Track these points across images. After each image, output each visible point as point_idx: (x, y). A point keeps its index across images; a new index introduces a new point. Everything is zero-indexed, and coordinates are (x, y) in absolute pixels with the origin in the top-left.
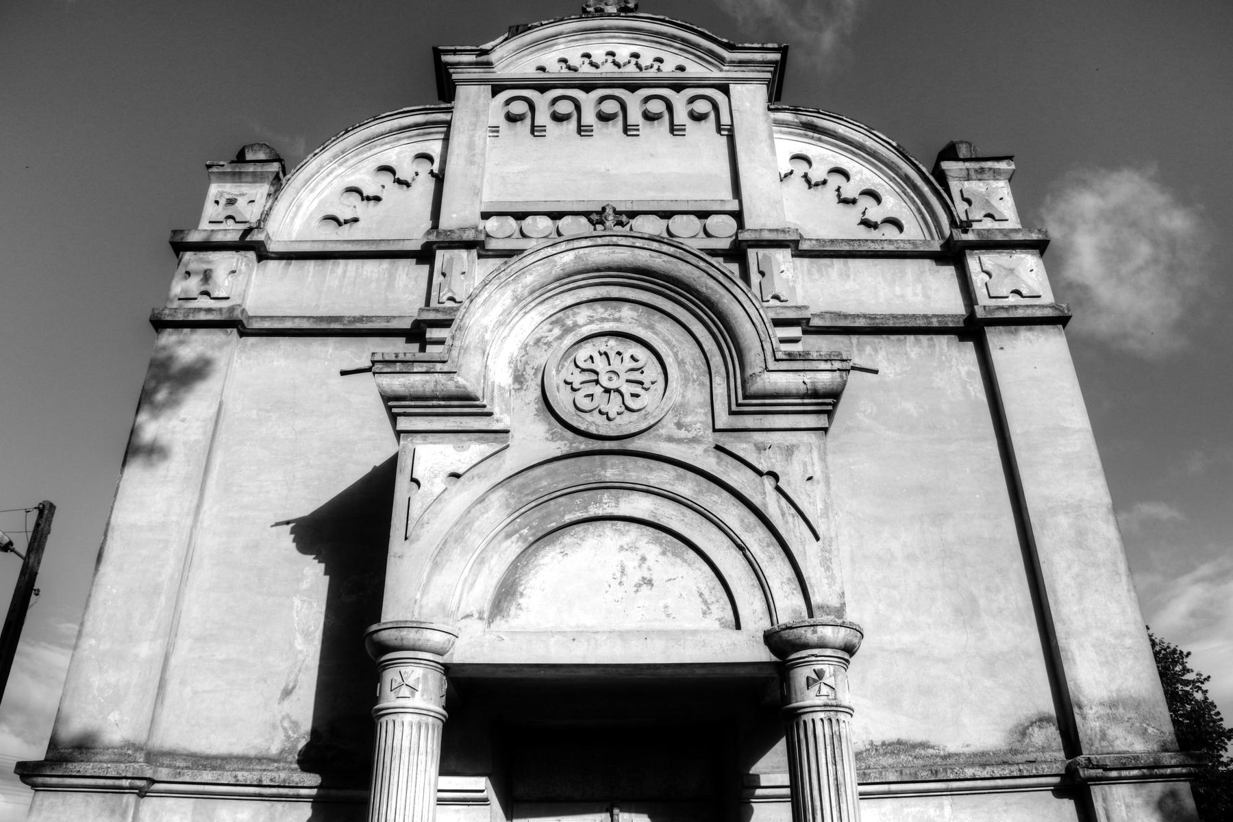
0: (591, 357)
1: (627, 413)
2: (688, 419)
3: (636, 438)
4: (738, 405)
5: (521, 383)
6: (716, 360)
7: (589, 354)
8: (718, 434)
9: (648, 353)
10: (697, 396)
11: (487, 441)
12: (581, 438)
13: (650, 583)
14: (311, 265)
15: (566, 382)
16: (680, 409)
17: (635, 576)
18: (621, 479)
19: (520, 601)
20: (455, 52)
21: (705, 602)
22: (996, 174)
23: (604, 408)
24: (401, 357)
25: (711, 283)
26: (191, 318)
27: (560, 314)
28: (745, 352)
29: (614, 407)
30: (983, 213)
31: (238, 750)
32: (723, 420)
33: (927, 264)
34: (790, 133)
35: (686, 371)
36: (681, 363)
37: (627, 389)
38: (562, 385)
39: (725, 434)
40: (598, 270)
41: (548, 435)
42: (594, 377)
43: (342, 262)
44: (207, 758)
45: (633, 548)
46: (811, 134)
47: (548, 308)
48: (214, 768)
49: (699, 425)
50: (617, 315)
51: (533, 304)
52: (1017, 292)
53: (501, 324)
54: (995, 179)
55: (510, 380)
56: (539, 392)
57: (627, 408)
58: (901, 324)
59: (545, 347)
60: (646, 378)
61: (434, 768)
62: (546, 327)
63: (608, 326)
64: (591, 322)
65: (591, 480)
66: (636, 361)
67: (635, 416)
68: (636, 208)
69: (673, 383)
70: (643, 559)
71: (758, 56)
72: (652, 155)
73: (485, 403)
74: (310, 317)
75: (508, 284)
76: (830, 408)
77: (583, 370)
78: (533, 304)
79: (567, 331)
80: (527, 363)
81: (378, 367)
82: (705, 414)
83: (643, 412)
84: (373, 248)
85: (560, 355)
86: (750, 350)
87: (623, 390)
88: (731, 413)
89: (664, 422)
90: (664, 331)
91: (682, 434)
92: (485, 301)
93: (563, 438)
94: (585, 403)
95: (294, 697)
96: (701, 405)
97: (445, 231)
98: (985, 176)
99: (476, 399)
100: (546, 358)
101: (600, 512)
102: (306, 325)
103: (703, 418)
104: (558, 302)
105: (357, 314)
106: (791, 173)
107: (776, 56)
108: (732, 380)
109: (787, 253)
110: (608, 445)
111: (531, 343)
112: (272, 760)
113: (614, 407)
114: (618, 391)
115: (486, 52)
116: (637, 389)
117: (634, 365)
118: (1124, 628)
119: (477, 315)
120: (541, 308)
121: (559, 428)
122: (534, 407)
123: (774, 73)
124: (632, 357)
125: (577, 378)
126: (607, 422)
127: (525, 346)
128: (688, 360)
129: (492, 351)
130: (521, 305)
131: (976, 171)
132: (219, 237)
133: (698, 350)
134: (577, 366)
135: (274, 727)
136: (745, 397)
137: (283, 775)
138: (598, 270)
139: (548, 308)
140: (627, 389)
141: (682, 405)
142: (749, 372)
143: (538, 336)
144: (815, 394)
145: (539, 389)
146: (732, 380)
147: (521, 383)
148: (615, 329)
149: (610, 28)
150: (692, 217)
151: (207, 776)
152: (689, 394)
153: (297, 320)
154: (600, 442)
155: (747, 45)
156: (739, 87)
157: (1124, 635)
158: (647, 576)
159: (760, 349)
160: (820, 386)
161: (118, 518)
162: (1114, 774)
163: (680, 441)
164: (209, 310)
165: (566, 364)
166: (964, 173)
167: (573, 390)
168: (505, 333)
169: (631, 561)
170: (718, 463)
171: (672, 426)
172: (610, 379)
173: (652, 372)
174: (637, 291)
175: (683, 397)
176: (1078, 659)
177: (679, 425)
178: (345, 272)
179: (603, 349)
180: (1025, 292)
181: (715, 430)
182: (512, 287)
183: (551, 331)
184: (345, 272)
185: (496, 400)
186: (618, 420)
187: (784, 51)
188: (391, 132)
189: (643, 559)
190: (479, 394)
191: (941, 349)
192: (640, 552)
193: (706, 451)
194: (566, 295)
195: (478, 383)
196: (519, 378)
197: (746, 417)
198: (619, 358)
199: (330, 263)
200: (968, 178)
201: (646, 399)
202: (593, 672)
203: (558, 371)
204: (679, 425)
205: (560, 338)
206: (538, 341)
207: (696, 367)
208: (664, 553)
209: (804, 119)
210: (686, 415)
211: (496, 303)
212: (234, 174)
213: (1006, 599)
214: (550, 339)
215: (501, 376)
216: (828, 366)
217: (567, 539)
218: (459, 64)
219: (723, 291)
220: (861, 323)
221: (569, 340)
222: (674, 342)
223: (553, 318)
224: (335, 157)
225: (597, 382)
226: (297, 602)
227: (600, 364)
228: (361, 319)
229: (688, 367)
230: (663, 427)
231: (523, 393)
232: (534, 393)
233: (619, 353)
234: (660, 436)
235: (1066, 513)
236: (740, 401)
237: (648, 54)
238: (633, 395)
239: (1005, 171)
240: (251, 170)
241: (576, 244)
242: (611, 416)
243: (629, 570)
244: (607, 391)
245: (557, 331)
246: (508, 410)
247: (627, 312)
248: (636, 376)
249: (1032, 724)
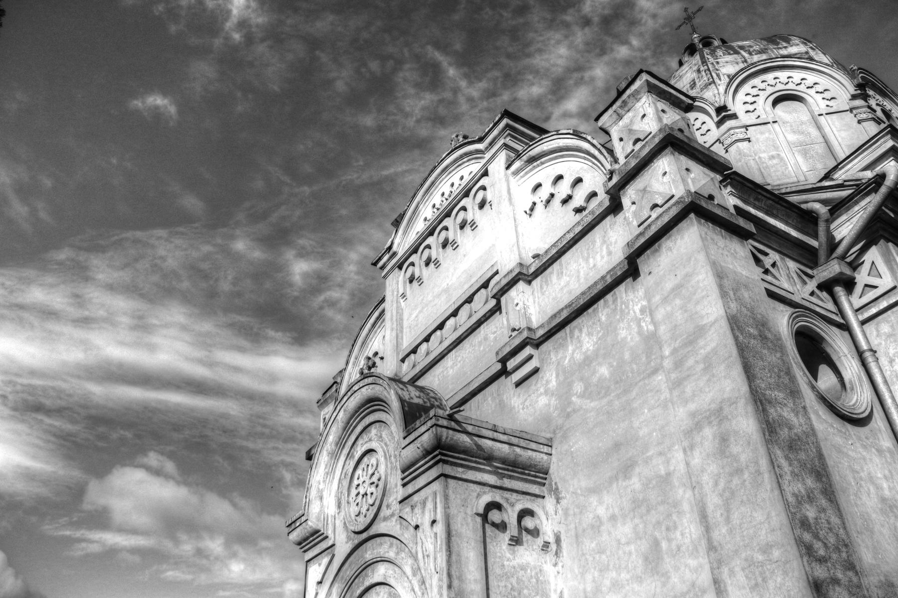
22: (636, 96)
30: (631, 143)
33: (609, 219)
34: (526, 173)
40: (356, 412)
46: (535, 164)
52: (655, 206)
54: (638, 100)
58: (587, 297)
71: (495, 132)
98: (630, 105)
106: (534, 204)
109: (521, 285)
115: (390, 248)
118: (770, 538)
131: (621, 107)
138: (356, 412)
149: (436, 178)
157: (771, 546)
166: (615, 116)
176: (729, 588)
180: (660, 202)
188: (370, 331)
191: (622, 298)
200: (620, 117)
213: (682, 534)
220: (565, 314)
224: (354, 364)
235: (710, 423)
237: (455, 179)
239: (641, 87)
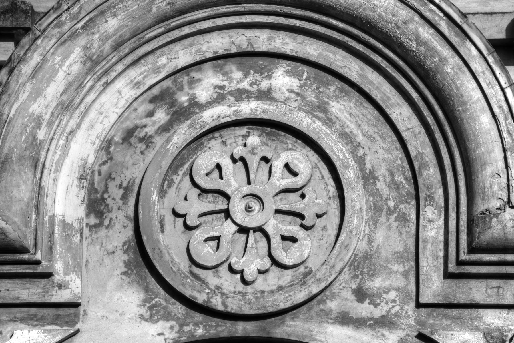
0: (218, 167)
1: (275, 270)
2: (376, 284)
3: (288, 316)
4: (460, 263)
5: (100, 215)
6: (430, 174)
7: (214, 161)
8: (424, 311)
9: (314, 157)
10: (391, 240)
12: (198, 317)
15: (175, 214)
16: (363, 264)
23: (237, 263)
25: (426, 33)
27: (168, 83)
28: (477, 167)
29: (253, 263)
32: (434, 287)
35: (377, 193)
36: (368, 178)
37: (275, 226)
38: (169, 218)
39: (436, 312)
41: (143, 311)
42: (221, 205)
47: (146, 75)
49: (393, 295)
50: (265, 85)
51: (120, 67)
53: (65, 107)
55: (81, 211)
56: (129, 232)
57: (275, 262)
59: (141, 146)
60: (308, 207)
61: (442, 278)
62: (143, 108)
63: (249, 108)
64: (220, 98)
66: (295, 174)
67: (288, 276)
69: (353, 220)
73: (38, 256)
75: (74, 35)
77: (204, 191)
78: (120, 67)
79: (180, 114)
80: (110, 177)
82: (405, 274)
83: (302, 269)
85: (166, 164)
86: (485, 164)
87: (270, 229)
88: (448, 275)
89: (335, 288)
90: (344, 117)
91: (365, 310)
92: (36, 70)
93: (168, 316)
94: (206, 253)
96: (400, 258)
99: (25, 250)
100: (142, 167)
103: (401, 282)
104: (163, 60)
108: (453, 215)
111: (117, 139)
113: (253, 263)
114: (260, 229)
116: (293, 228)
117: (289, 181)
119: (23, 97)
120: (134, 73)
121: (161, 297)
122: (121, 258)
124: (287, 166)
125: (195, 207)
126: (240, 287)
127: (107, 145)
128: (382, 172)
129: (51, 158)
130: (99, 70)
133: (399, 153)
134: (195, 184)
136: (472, 250)
139: (146, 75)
140: (275, 226)
141: (367, 257)
142: (480, 207)
143: (129, 124)
145: (131, 226)
146: (453, 215)
147: (100, 215)
148: (259, 115)
152: (380, 236)
154: (229, 323)
159: (501, 164)
165: (177, 179)
167: (188, 228)
168: (72, 124)
171: (348, 295)
172: (248, 209)
173: (319, 196)
174: (301, 38)
175: (370, 241)
177: (361, 294)
179: (239, 151)
181: (419, 305)
182: (82, 41)
183: (151, 114)
185: (58, 249)
186: (261, 284)
190: (29, 242)
194: (177, 47)
195: (27, 223)
196: (96, 205)
197: (473, 283)
198: (265, 167)
201: (307, 247)
203: (163, 193)
204: (361, 294)
205: (166, 128)
206: (129, 135)
207: (394, 185)
210: (372, 275)
211: (55, 72)
214: (150, 130)
215: (66, 201)
219: (445, 51)
221: (182, 135)
222: (360, 138)
223: (155, 91)
225: (227, 214)
227: (233, 181)
229: (381, 185)
230: (333, 297)
231: (103, 232)
232: (120, 234)
233: (265, 160)
234: (327, 313)
236: (463, 257)
238: (284, 238)
242: (248, 277)
244: (243, 230)
245: (161, 116)
246: (77, 267)
247: (282, 80)
248: (292, 202)
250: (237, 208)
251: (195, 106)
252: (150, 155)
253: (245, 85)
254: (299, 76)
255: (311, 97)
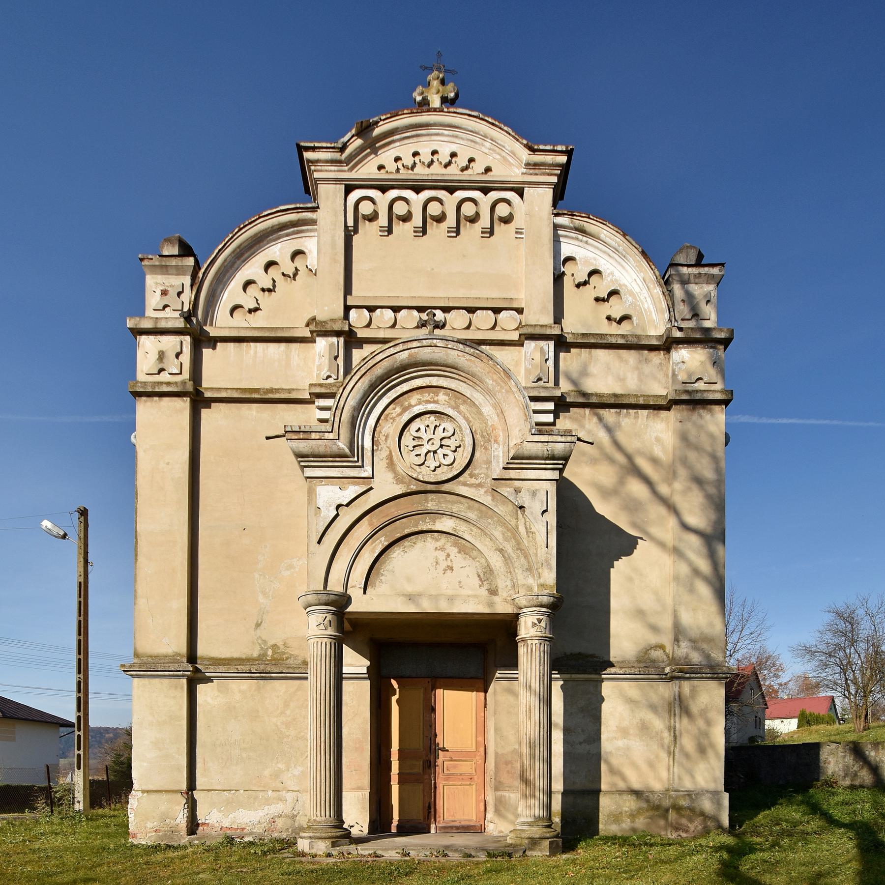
11: (358, 484)
13: (451, 569)
14: (231, 345)
17: (443, 565)
18: (436, 508)
19: (382, 578)
20: (314, 149)
21: (481, 580)
24: (303, 429)
26: (157, 390)
31: (236, 655)
43: (252, 344)
44: (220, 659)
45: (442, 549)
46: (580, 237)
48: (225, 665)
50: (436, 398)
64: (420, 404)
65: (420, 508)
68: (451, 305)
70: (448, 555)
72: (464, 256)
74: (237, 389)
76: (561, 466)
81: (289, 436)
84: (273, 334)
95: (262, 627)
97: (321, 322)
101: (425, 528)
102: (236, 395)
105: (268, 386)
107: (563, 159)
110: (430, 487)
112: (255, 660)
123: (559, 176)
131: (695, 275)
132: (163, 325)
135: (253, 643)
137: (262, 667)
144: (553, 457)
150: (490, 312)
151: (222, 669)
153: (229, 391)
155: (541, 147)
156: (532, 190)
158: (450, 564)
160: (556, 453)
161: (140, 527)
162: (688, 675)
163: (471, 486)
164: (168, 384)
169: (441, 556)
170: (493, 500)
178: (256, 352)
181: (181, 373)
184: (256, 352)
187: (569, 153)
189: (448, 555)
192: (447, 551)
193: (485, 492)
199: (244, 345)
202: (420, 616)
208: (459, 552)
209: (577, 223)
212: (162, 267)
214: (394, 415)
216: (563, 439)
217: (406, 543)
218: (318, 161)
222: (471, 419)
225: (435, 452)
226: (257, 576)
228: (271, 391)
240: (174, 264)
241: (410, 345)
243: (441, 562)
249: (651, 648)
250: (433, 448)
251: (410, 406)
252: (395, 424)
253: (429, 398)
254: (448, 395)
255: (453, 403)
